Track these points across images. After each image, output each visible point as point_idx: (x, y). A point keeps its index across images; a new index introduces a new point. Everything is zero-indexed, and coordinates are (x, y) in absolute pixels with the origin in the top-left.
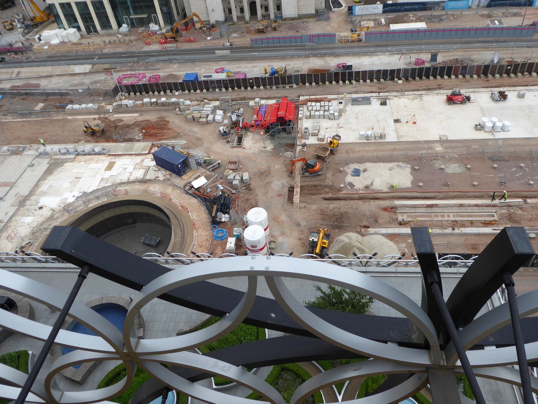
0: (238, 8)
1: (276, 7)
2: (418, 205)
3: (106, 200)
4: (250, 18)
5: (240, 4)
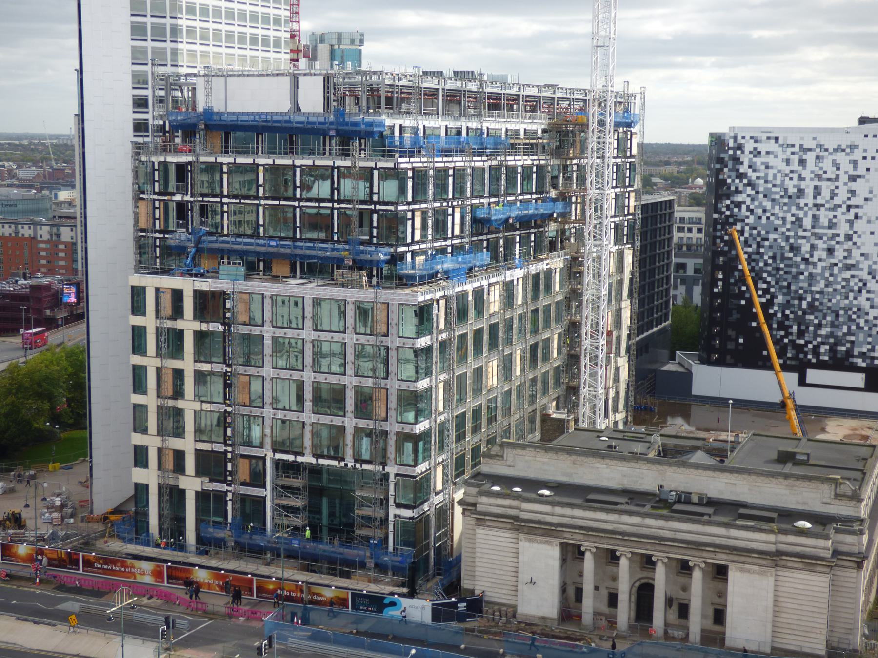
0: (604, 593)
1: (710, 612)
2: (182, 384)
3: (495, 362)
4: (631, 627)
5: (610, 584)
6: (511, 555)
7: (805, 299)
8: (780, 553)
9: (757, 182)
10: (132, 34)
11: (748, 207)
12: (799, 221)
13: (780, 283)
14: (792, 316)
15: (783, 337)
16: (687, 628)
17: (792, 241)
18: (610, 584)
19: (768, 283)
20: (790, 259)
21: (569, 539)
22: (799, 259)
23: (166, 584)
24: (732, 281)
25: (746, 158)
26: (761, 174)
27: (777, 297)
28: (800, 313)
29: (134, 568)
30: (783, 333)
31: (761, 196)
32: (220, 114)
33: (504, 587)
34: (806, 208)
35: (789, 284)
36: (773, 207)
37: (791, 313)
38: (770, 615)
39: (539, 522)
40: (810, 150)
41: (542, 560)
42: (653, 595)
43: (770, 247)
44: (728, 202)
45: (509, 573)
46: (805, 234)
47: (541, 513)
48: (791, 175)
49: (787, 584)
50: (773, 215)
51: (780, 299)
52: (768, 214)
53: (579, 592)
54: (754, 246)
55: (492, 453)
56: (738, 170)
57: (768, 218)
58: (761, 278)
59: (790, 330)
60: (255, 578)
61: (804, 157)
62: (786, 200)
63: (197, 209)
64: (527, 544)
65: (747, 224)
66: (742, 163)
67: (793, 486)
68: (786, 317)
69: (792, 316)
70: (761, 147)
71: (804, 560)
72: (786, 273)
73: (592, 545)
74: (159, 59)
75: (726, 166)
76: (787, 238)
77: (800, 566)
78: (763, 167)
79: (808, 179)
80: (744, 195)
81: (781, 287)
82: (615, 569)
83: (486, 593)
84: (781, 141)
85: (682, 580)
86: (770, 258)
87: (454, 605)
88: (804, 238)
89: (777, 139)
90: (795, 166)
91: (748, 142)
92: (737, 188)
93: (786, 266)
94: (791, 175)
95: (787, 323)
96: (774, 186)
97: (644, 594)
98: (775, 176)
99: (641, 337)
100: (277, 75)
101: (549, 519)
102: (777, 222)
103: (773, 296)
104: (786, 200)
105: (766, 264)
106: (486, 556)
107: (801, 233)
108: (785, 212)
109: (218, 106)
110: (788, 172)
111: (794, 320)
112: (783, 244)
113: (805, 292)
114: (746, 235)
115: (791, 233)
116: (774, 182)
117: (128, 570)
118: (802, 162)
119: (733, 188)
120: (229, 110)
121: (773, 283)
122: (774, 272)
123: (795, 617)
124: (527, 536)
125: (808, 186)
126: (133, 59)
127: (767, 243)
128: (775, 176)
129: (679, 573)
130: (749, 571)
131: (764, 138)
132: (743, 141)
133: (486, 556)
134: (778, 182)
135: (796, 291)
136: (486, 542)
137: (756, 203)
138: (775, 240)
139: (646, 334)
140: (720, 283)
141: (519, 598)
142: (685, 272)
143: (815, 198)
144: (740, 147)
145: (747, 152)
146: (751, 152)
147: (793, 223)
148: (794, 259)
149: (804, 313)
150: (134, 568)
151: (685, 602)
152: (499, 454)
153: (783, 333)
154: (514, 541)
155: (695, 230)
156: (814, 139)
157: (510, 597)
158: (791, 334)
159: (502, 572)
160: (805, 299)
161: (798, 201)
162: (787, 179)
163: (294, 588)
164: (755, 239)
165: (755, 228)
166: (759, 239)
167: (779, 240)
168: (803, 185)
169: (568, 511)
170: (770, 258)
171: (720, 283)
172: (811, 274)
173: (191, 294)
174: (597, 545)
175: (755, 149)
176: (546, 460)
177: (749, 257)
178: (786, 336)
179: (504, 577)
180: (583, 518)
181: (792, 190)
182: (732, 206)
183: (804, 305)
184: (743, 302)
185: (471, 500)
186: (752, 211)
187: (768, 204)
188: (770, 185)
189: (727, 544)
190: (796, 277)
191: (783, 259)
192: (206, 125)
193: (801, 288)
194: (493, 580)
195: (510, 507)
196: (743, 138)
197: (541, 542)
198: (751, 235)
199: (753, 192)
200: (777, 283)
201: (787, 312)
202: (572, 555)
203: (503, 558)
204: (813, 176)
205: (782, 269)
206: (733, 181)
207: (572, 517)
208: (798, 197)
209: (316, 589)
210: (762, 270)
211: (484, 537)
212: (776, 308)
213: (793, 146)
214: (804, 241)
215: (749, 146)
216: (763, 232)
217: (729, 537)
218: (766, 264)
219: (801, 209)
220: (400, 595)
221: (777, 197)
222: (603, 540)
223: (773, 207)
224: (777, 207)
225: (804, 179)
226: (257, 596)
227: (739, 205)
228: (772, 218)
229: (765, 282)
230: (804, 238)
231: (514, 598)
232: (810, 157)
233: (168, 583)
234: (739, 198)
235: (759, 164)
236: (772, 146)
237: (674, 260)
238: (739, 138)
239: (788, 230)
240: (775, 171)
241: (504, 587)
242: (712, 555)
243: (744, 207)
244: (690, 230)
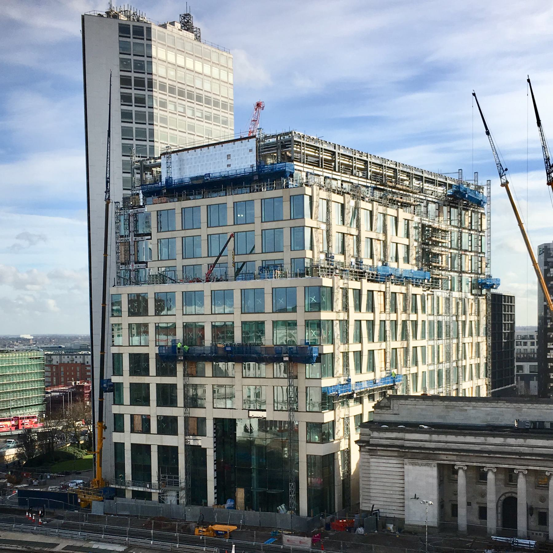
0: (475, 507)
5: (479, 499)
6: (399, 477)
18: (479, 499)
33: (393, 504)
39: (420, 448)
41: (423, 478)
45: (397, 493)
47: (421, 441)
53: (455, 508)
64: (411, 467)
73: (464, 464)
74: (141, 134)
82: (483, 487)
85: (539, 492)
97: (508, 505)
99: (493, 390)
101: (427, 445)
106: (378, 480)
124: (410, 461)
126: (123, 169)
133: (378, 480)
136: (378, 468)
141: (406, 513)
155: (529, 343)
157: (399, 512)
169: (443, 438)
173: (159, 378)
185: (366, 438)
194: (385, 499)
197: (422, 465)
202: (446, 475)
207: (447, 442)
222: (474, 460)
237: (516, 364)
241: (393, 504)
244: (525, 344)
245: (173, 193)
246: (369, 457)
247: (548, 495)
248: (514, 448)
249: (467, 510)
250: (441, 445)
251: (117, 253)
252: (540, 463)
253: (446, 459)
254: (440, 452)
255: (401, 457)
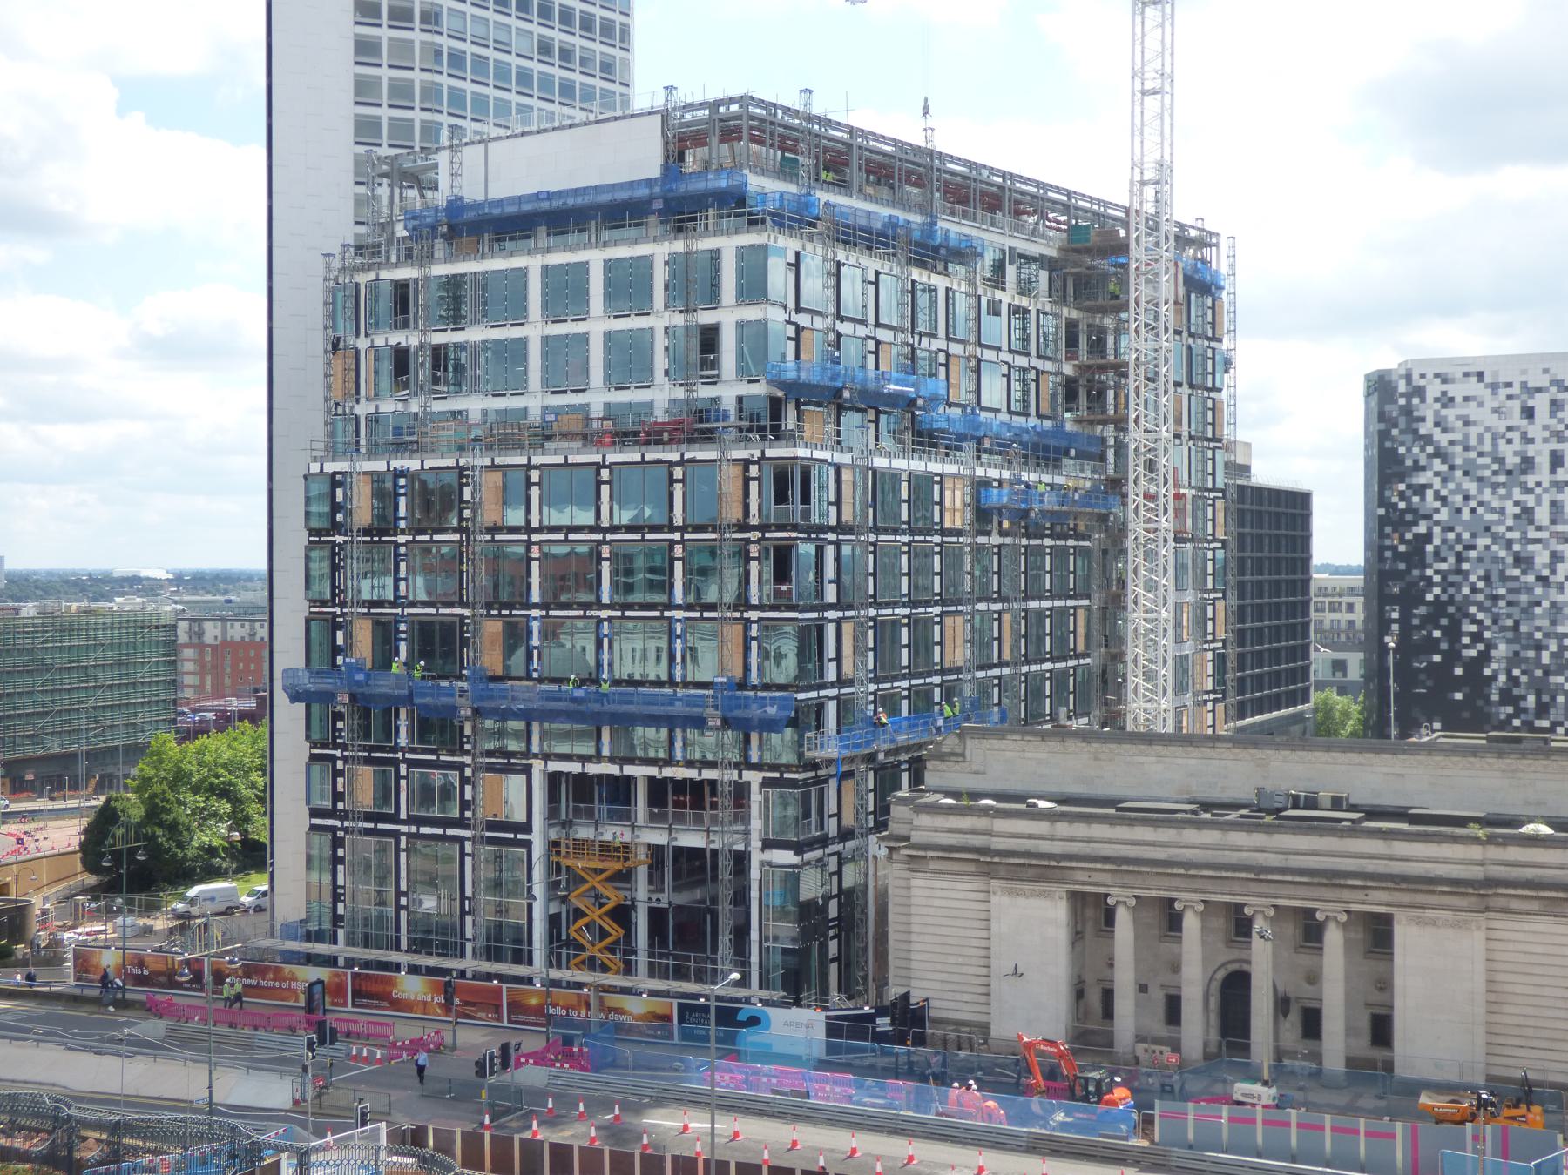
0: (1158, 996)
1: (1364, 1023)
7: (1547, 648)
8: (1491, 882)
9: (1450, 449)
10: (356, 135)
11: (1437, 493)
12: (1527, 514)
13: (1501, 623)
14: (1524, 679)
15: (1510, 717)
16: (1317, 1057)
17: (1516, 547)
19: (1480, 623)
20: (1516, 579)
21: (1083, 884)
22: (1531, 579)
23: (350, 1008)
24: (1416, 622)
25: (1429, 410)
26: (1457, 436)
27: (1496, 647)
28: (1538, 673)
29: (295, 980)
30: (1510, 710)
31: (1458, 473)
32: (475, 206)
33: (965, 988)
34: (1538, 491)
35: (1517, 623)
36: (1480, 491)
37: (1524, 673)
38: (1481, 1010)
39: (1027, 854)
40: (1539, 390)
41: (1035, 925)
42: (1248, 996)
43: (1480, 560)
44: (1402, 487)
46: (1539, 535)
47: (1030, 837)
48: (1509, 435)
49: (1511, 947)
50: (1481, 504)
51: (1502, 650)
52: (1473, 504)
53: (1108, 996)
54: (1452, 560)
55: (945, 749)
56: (1416, 431)
57: (1473, 511)
58: (1467, 615)
59: (1522, 704)
60: (504, 986)
61: (1530, 403)
62: (1502, 479)
63: (424, 358)
64: (1006, 900)
65: (1437, 523)
66: (1423, 419)
67: (1515, 771)
68: (1514, 681)
69: (1524, 679)
70: (1455, 390)
71: (1542, 894)
72: (1510, 604)
75: (1396, 426)
76: (1509, 544)
77: (1535, 906)
78: (1459, 424)
79: (1538, 440)
80: (1429, 474)
81: (1504, 629)
83: (932, 1003)
84: (1488, 379)
85: (1305, 960)
86: (1480, 579)
87: (869, 1018)
88: (1538, 541)
89: (1480, 375)
90: (1517, 419)
91: (1430, 382)
92: (1416, 462)
93: (1510, 591)
94: (1509, 435)
95: (1516, 691)
96: (1481, 454)
97: (1234, 991)
98: (1480, 438)
100: (570, 126)
102: (1489, 517)
103: (1490, 646)
104: (1502, 479)
105: (1474, 590)
107: (1532, 534)
108: (1502, 498)
109: (472, 192)
110: (1503, 429)
111: (1529, 686)
112: (1502, 554)
113: (1547, 635)
114: (1437, 541)
115: (1516, 535)
116: (1480, 449)
117: (285, 985)
118: (1529, 413)
119: (1409, 462)
120: (491, 196)
121: (1488, 622)
122: (1488, 603)
123: (1530, 1011)
124: (1005, 884)
125: (1541, 453)
127: (1473, 554)
128: (1480, 438)
129: (1298, 949)
130: (1433, 923)
131: (1459, 375)
132: (1422, 382)
134: (1487, 447)
135: (1530, 635)
137: (1451, 486)
138: (1487, 548)
139: (1266, 716)
140: (1395, 627)
141: (994, 1008)
142: (1345, 675)
143: (1553, 471)
144: (1420, 392)
145: (1429, 399)
146: (1436, 400)
147: (1516, 516)
148: (1523, 579)
149: (1547, 673)
150: (295, 980)
151: (1314, 1005)
152: (958, 750)
153: (1510, 710)
154: (981, 896)
156: (1546, 371)
158: (1525, 710)
159: (960, 960)
160: (1547, 648)
161: (1523, 478)
162: (1502, 442)
163: (574, 1002)
164: (1451, 548)
165: (1451, 529)
166: (1459, 548)
167: (1495, 548)
168: (1531, 450)
169: (1080, 830)
170: (1480, 579)
171: (1395, 627)
172: (1553, 604)
174: (1137, 892)
175: (1444, 393)
176: (1043, 756)
177: (1444, 578)
178: (1516, 715)
179: (965, 969)
180: (1110, 842)
181: (1512, 461)
182: (1409, 493)
183: (1546, 658)
184: (1437, 658)
186: (1444, 500)
187: (1472, 488)
188: (1473, 454)
189: (1388, 871)
190: (1527, 611)
191: (1504, 578)
192: (451, 227)
193: (1539, 629)
194: (945, 977)
195: (973, 832)
196: (1423, 376)
197: (1032, 894)
198: (1444, 541)
199: (1445, 468)
200: (1495, 622)
201: (1516, 672)
202: (1091, 915)
203: (962, 932)
204: (1547, 434)
205: (1502, 597)
206: (1409, 450)
207: (1090, 841)
208: (1524, 472)
209: (614, 1000)
210: (1467, 601)
211: (927, 893)
212: (1495, 666)
213: (1509, 385)
214: (1538, 547)
215: (1434, 389)
216: (1466, 536)
217: (1391, 858)
218: (1474, 590)
219: (1530, 491)
220: (766, 1003)
221: (1487, 473)
223: (1480, 491)
224: (1488, 491)
225: (1532, 441)
226: (510, 1021)
227: (1421, 490)
228: (1480, 510)
229: (1474, 621)
230: (1538, 541)
231: (984, 1009)
232: (1541, 403)
233: (354, 1005)
234: (1422, 478)
235: (1451, 419)
236: (1473, 387)
238: (1415, 377)
239: (1509, 529)
240: (1481, 430)
242: (1360, 895)
243: (1429, 494)
245: (623, 219)
246: (908, 874)
247: (1321, 968)
248: (1245, 854)
249: (1137, 1005)
250: (1075, 847)
251: (326, 376)
252: (1303, 891)
253: (1090, 881)
254: (1074, 864)
255: (986, 874)
